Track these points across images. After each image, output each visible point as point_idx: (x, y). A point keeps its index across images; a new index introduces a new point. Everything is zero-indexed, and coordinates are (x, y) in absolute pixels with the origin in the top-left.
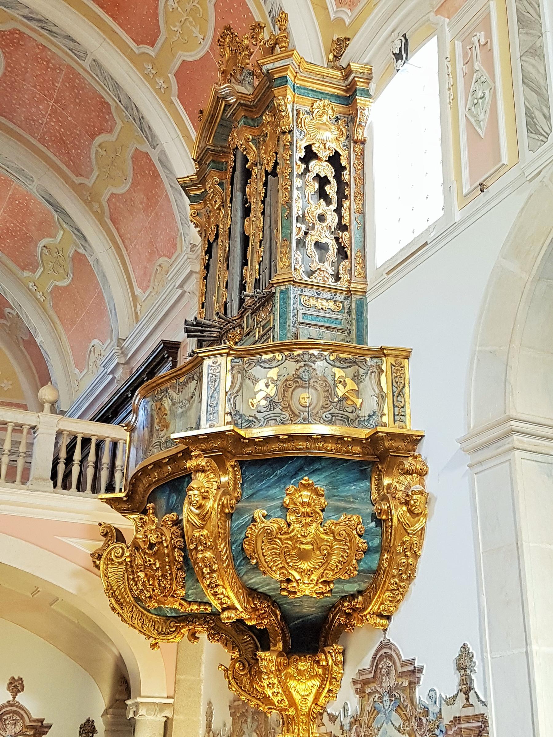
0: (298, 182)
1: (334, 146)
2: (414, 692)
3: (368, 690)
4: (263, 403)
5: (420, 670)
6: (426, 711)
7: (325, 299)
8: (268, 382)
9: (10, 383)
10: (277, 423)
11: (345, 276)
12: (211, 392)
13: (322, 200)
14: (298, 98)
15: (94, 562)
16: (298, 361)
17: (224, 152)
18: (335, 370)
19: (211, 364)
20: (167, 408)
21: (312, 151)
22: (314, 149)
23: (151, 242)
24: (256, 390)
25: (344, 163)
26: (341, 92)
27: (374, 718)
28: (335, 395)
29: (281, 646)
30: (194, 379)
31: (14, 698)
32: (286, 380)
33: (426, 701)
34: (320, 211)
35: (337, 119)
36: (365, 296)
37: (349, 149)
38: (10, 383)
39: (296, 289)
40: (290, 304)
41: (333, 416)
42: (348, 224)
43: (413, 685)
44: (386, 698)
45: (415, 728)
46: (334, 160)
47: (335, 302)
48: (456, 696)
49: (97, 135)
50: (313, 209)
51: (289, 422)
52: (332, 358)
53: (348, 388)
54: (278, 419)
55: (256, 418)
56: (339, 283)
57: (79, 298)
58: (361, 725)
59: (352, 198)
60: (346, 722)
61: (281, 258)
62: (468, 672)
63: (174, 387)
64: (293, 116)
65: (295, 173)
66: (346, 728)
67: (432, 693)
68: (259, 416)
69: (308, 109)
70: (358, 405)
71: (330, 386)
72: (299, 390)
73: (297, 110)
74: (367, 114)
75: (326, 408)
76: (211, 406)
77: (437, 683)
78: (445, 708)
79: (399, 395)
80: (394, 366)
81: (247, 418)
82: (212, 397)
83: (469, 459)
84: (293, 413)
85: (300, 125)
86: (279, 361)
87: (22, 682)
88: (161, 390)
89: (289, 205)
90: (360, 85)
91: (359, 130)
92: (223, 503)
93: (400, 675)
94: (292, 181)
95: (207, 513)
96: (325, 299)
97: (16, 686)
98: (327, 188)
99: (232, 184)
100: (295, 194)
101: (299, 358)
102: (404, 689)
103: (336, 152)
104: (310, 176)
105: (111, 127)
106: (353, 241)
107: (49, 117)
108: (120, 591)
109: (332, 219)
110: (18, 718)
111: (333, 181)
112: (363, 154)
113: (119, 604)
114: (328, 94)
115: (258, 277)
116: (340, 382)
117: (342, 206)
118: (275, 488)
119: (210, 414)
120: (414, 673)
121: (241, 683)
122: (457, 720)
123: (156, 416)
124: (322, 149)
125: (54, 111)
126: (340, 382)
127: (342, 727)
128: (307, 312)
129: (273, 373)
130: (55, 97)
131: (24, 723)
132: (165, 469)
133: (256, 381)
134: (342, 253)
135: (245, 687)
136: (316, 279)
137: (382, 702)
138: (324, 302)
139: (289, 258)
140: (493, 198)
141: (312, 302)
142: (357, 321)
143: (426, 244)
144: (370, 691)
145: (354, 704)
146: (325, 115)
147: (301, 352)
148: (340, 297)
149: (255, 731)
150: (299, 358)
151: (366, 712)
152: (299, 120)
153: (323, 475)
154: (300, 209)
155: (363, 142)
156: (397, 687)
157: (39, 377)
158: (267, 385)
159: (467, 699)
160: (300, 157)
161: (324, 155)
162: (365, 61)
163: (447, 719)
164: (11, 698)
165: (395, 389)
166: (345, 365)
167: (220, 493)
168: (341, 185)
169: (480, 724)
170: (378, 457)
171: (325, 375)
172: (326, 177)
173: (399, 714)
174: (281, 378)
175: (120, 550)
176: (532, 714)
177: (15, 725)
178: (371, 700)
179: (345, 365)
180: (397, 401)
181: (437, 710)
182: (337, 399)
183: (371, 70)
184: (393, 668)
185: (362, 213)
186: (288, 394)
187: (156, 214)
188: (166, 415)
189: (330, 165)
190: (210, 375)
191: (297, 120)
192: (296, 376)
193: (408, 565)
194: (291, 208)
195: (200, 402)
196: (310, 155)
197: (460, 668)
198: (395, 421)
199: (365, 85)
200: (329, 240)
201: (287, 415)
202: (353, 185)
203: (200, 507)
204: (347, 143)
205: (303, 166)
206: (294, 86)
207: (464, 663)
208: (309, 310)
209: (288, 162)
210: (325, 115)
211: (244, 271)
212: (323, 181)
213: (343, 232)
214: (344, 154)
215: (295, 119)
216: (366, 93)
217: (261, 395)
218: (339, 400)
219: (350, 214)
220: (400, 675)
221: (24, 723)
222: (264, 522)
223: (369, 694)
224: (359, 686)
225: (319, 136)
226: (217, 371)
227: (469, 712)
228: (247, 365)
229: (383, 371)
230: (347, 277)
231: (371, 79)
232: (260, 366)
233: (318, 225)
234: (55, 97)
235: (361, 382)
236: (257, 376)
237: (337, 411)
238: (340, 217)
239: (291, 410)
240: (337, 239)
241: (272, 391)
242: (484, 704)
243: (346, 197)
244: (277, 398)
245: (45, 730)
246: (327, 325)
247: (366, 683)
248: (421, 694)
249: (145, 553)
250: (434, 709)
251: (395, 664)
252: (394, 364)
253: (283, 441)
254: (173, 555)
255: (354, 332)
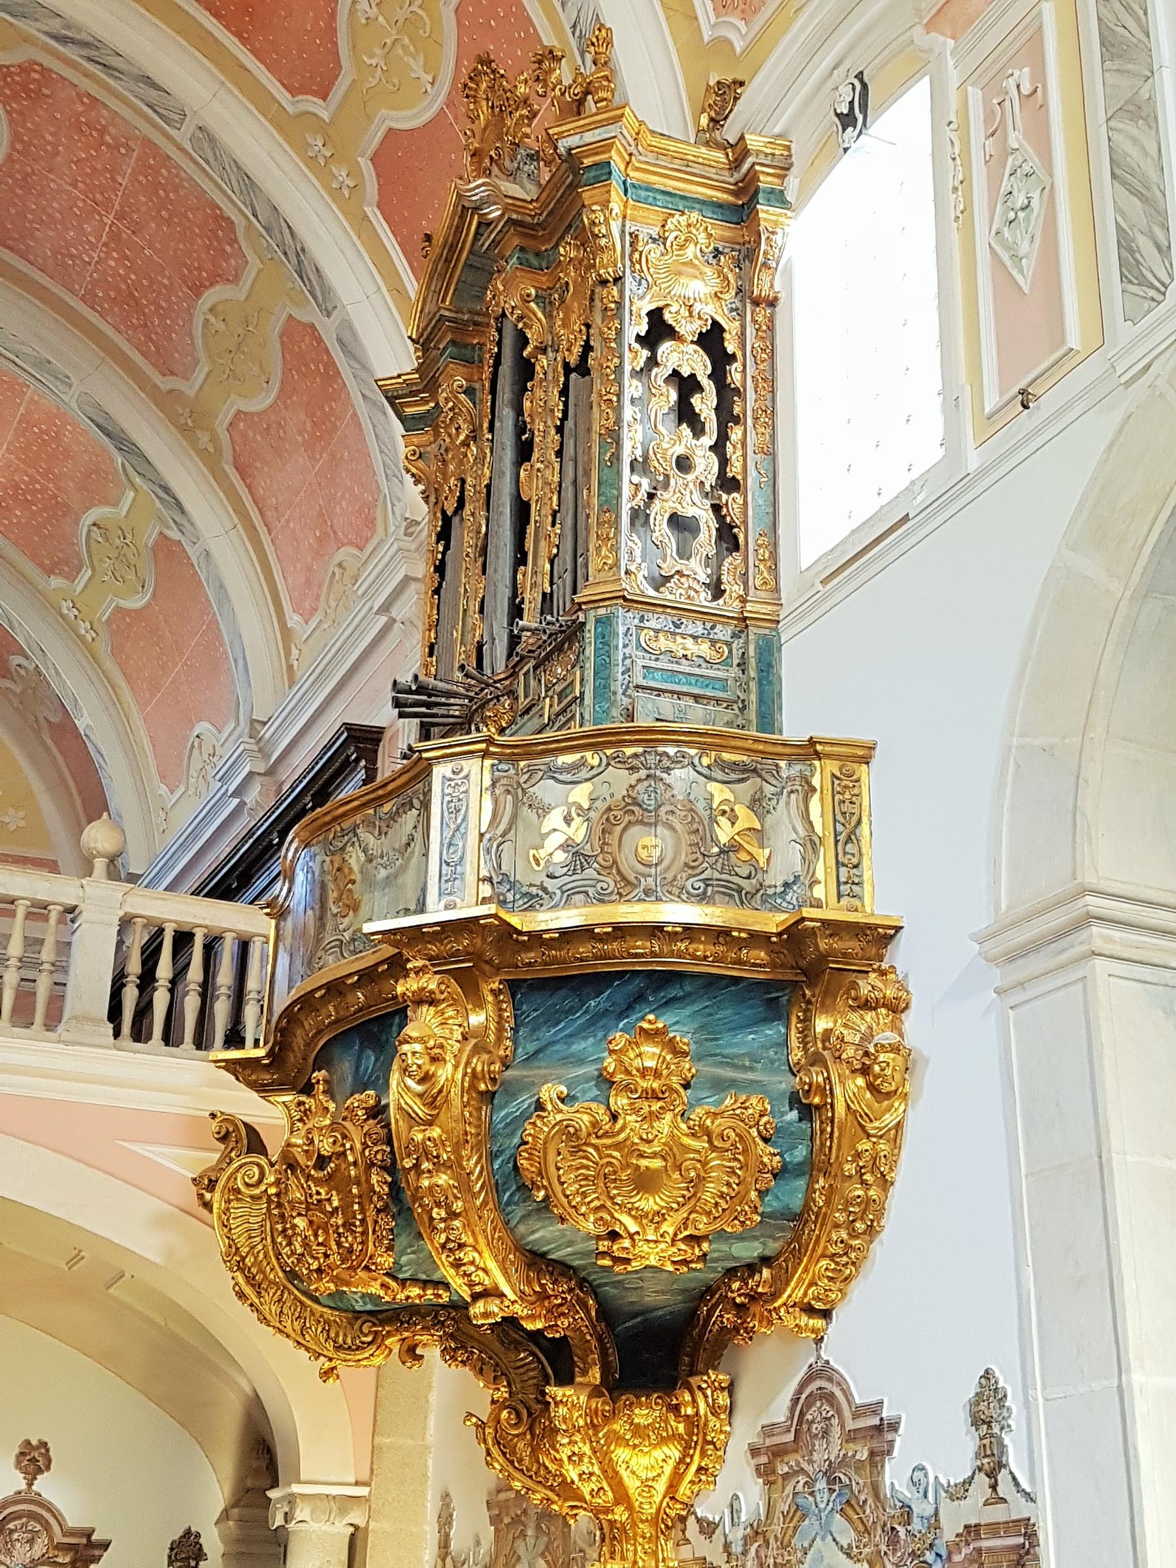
0: (633, 388)
1: (711, 310)
2: (881, 1473)
3: (782, 1469)
4: (560, 857)
5: (894, 1426)
6: (907, 1513)
7: (691, 636)
8: (569, 813)
9: (22, 814)
10: (589, 900)
11: (733, 588)
12: (448, 834)
13: (685, 425)
14: (634, 208)
15: (201, 1196)
16: (633, 769)
17: (476, 324)
18: (713, 787)
19: (449, 775)
20: (356, 868)
21: (664, 322)
22: (668, 317)
23: (320, 514)
24: (544, 830)
25: (731, 347)
26: (725, 196)
27: (796, 1528)
28: (712, 840)
29: (598, 1375)
30: (412, 806)
31: (30, 1485)
32: (609, 809)
33: (905, 1492)
34: (680, 450)
35: (717, 253)
36: (776, 629)
37: (742, 316)
38: (22, 814)
39: (630, 614)
40: (617, 647)
41: (707, 885)
42: (739, 477)
43: (877, 1457)
44: (821, 1484)
45: (883, 1548)
46: (711, 340)
47: (713, 642)
48: (969, 1481)
49: (207, 287)
50: (665, 445)
51: (614, 897)
52: (706, 761)
53: (739, 825)
54: (591, 891)
55: (545, 890)
56: (721, 601)
57: (168, 635)
58: (767, 1542)
59: (750, 421)
60: (736, 1536)
61: (598, 549)
62: (996, 1429)
63: (369, 824)
64: (623, 247)
65: (627, 368)
66: (737, 1548)
67: (918, 1475)
68: (550, 884)
69: (655, 231)
70: (762, 862)
71: (701, 822)
72: (636, 829)
73: (631, 234)
74: (779, 242)
75: (693, 868)
76: (448, 864)
77: (930, 1454)
78: (946, 1506)
79: (849, 840)
80: (838, 778)
81: (525, 889)
82: (450, 844)
83: (997, 976)
84: (624, 878)
85: (637, 266)
86: (592, 768)
87: (48, 1450)
88: (342, 830)
89: (614, 436)
90: (766, 181)
91: (763, 276)
92: (474, 1069)
93: (852, 1437)
94: (621, 386)
95: (440, 1091)
96: (691, 636)
97: (33, 1460)
98: (696, 400)
99: (493, 391)
100: (628, 412)
101: (635, 762)
102: (859, 1466)
103: (715, 323)
104: (660, 374)
105: (236, 271)
106: (750, 513)
107: (104, 249)
108: (256, 1258)
109: (706, 466)
110: (39, 1527)
111: (708, 385)
112: (771, 329)
113: (253, 1286)
114: (697, 201)
115: (548, 590)
116: (724, 813)
117: (727, 438)
118: (585, 1038)
119: (446, 881)
120: (880, 1433)
121: (513, 1452)
122: (972, 1531)
123: (331, 886)
124: (685, 318)
125: (115, 236)
126: (724, 813)
127: (727, 1546)
128: (653, 664)
129: (581, 794)
130: (117, 206)
131: (51, 1539)
132: (350, 999)
133: (544, 810)
134: (728, 538)
135: (520, 1461)
136: (671, 594)
137: (812, 1494)
138: (689, 642)
139: (615, 549)
140: (1048, 422)
141: (663, 643)
142: (760, 683)
143: (906, 519)
144: (786, 1469)
145: (752, 1497)
146: (692, 245)
147: (640, 750)
148: (723, 633)
149: (543, 1555)
150: (635, 762)
151: (778, 1514)
152: (637, 255)
153: (687, 1012)
154: (639, 445)
155: (772, 303)
156: (844, 1462)
157: (83, 802)
158: (568, 820)
159: (994, 1487)
160: (638, 335)
161: (689, 329)
162: (776, 131)
163: (950, 1530)
164: (23, 1485)
165: (840, 828)
166: (733, 776)
167: (469, 1048)
168: (726, 393)
169: (1021, 1540)
170: (804, 972)
171: (692, 798)
172: (693, 376)
173: (849, 1520)
174: (598, 804)
175: (256, 1169)
176: (1132, 1520)
177: (31, 1542)
178: (789, 1489)
179: (733, 776)
180: (845, 853)
181: (930, 1511)
182: (716, 850)
183: (788, 148)
184: (835, 1421)
185: (770, 452)
186: (613, 839)
187: (333, 455)
188: (354, 882)
189: (702, 352)
190: (447, 798)
191: (631, 256)
192: (629, 800)
193: (868, 1202)
194: (618, 442)
195: (426, 855)
196: (659, 330)
197: (979, 1420)
198: (839, 896)
199: (776, 180)
200: (700, 511)
201: (610, 883)
202: (750, 395)
203: (425, 1079)
204: (739, 304)
205: (645, 353)
206: (624, 183)
207: (986, 1410)
208: (657, 660)
209: (613, 345)
210: (692, 245)
211: (519, 576)
212: (687, 386)
213: (729, 493)
214: (731, 327)
215: (627, 253)
216: (779, 198)
217: (556, 840)
218: (722, 852)
219: (745, 456)
220: (852, 1437)
221: (51, 1539)
222: (561, 1111)
223: (786, 1477)
224: (764, 1459)
225: (678, 290)
226: (462, 789)
227: (998, 1514)
228: (526, 777)
229: (814, 790)
230: (738, 589)
231: (788, 169)
232: (553, 778)
233: (677, 479)
234: (117, 206)
235: (768, 812)
236: (547, 801)
237: (717, 875)
238: (724, 462)
239: (619, 872)
240: (716, 508)
241: (578, 831)
242: (1029, 1497)
243: (737, 420)
244: (588, 846)
245: (97, 1553)
246: (696, 691)
247: (778, 1452)
248: (895, 1476)
249: (309, 1177)
250: (923, 1509)
251: (839, 1412)
252: (838, 774)
253: (603, 938)
254: (368, 1180)
255: (753, 707)
